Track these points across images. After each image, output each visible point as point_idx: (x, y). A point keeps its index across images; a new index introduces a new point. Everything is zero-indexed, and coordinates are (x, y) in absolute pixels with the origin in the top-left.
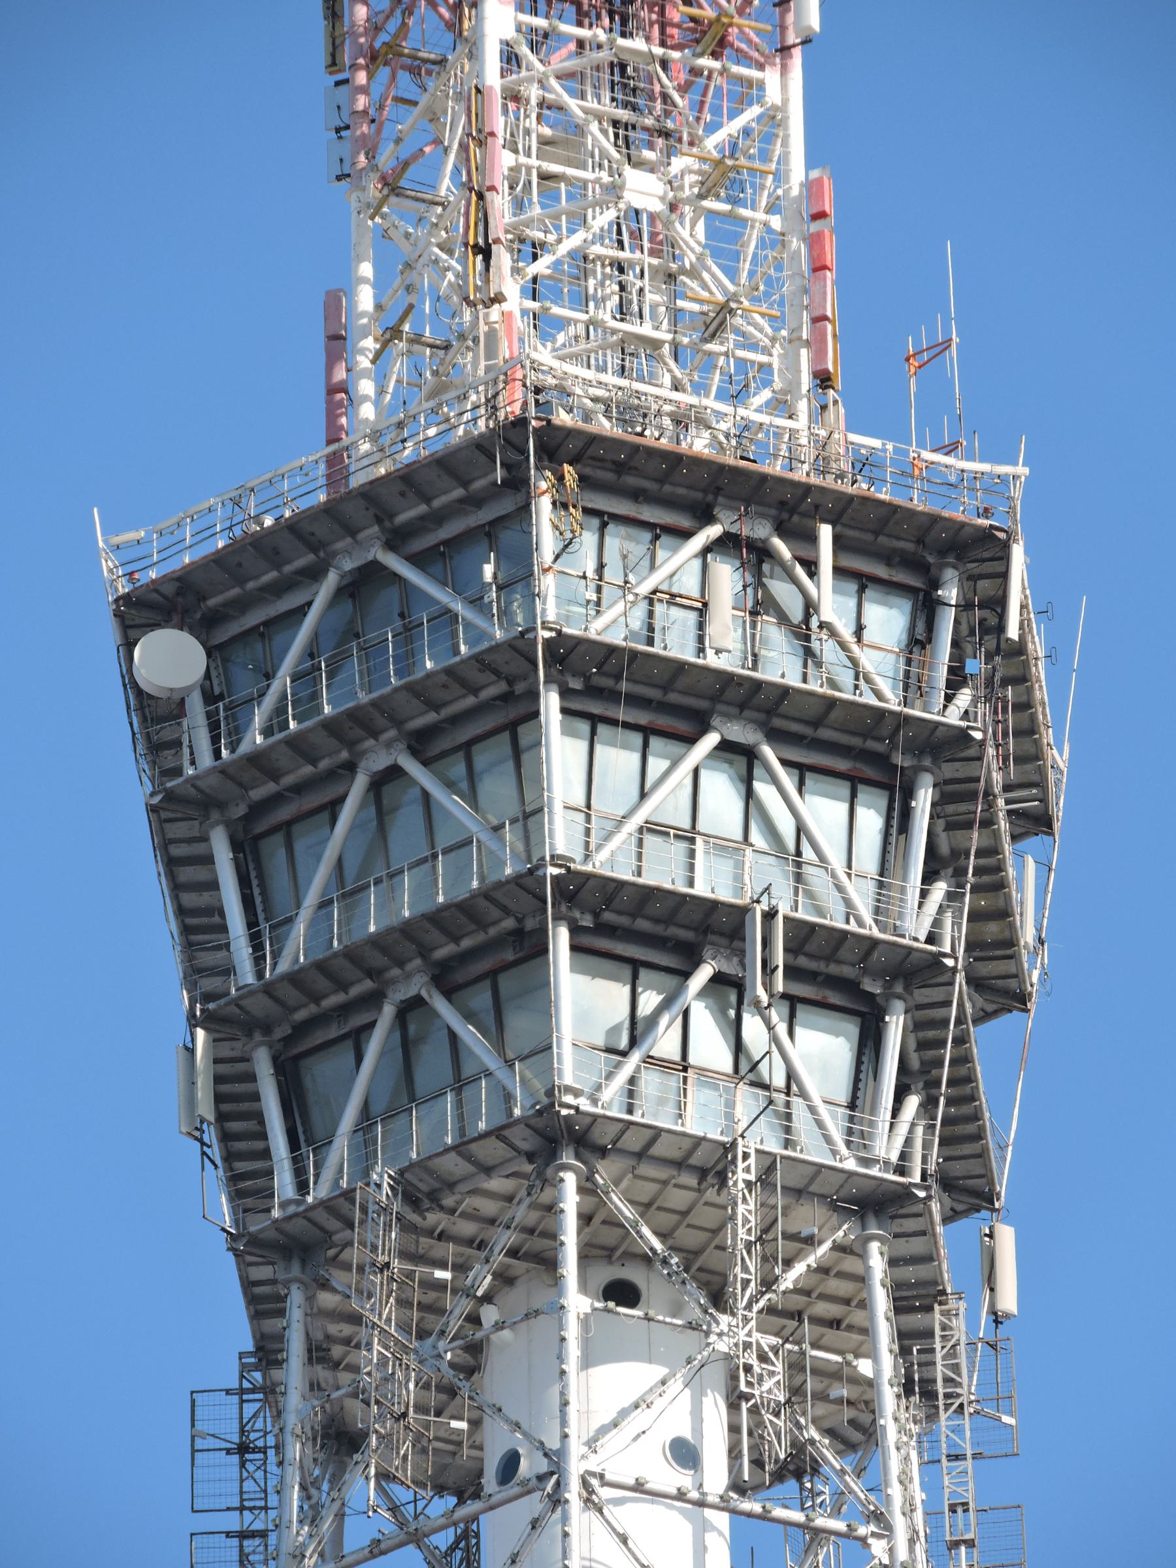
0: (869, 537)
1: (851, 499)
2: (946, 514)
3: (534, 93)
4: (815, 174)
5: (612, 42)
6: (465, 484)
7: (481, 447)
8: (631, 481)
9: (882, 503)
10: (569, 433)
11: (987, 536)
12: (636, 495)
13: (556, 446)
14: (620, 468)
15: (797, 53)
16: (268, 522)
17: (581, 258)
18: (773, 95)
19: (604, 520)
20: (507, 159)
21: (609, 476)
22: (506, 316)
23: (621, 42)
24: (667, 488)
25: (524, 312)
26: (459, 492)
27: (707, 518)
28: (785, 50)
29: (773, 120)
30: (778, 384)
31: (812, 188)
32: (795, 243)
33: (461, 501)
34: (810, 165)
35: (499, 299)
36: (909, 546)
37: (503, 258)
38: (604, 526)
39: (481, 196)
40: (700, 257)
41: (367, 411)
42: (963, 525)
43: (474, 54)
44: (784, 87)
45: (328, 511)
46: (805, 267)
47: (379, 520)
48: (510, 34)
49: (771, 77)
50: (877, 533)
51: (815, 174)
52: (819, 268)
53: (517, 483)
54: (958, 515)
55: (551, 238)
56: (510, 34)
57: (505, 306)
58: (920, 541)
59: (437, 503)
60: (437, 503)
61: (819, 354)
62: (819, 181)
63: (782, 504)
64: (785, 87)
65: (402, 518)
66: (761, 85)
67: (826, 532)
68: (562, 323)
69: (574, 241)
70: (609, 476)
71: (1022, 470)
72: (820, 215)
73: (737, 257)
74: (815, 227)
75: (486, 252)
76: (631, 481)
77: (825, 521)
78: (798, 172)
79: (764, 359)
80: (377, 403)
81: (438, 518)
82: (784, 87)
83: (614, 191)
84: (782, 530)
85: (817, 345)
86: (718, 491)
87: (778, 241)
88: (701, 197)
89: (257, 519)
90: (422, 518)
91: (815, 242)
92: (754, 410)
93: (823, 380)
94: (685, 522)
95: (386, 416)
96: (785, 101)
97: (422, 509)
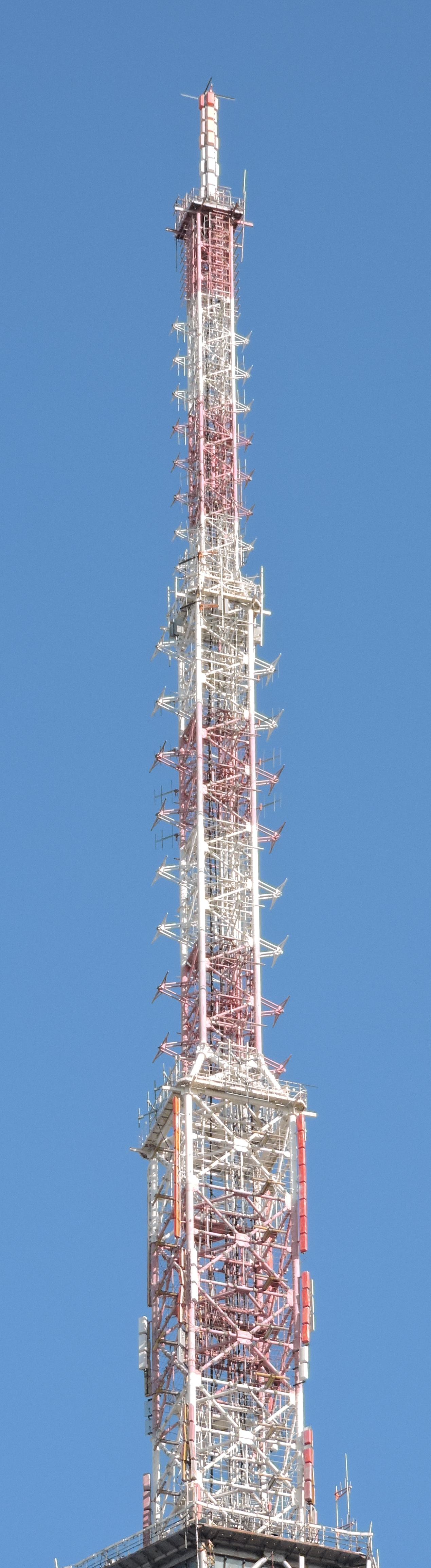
0: (317, 1559)
1: (310, 1547)
2: (344, 1551)
3: (210, 1404)
4: (306, 1429)
5: (235, 1386)
6: (177, 1547)
7: (181, 1535)
8: (234, 1544)
9: (321, 1548)
10: (211, 1529)
11: (359, 1558)
12: (237, 1549)
13: (206, 1534)
14: (230, 1540)
15: (301, 1386)
16: (113, 1561)
17: (228, 1461)
18: (292, 1402)
19: (225, 1558)
20: (198, 1428)
21: (226, 1543)
22: (197, 1485)
23: (238, 1385)
24: (247, 1546)
25: (205, 1483)
26: (175, 1550)
27: (261, 1555)
28: (296, 1385)
29: (293, 1409)
30: (293, 1503)
31: (305, 1434)
32: (300, 1453)
33: (177, 1553)
34: (305, 1426)
35: (193, 1479)
36: (333, 1562)
37: (194, 1463)
38: (225, 1560)
39: (188, 1443)
40: (266, 1460)
41: (158, 1516)
42: (350, 1554)
43: (186, 1394)
44: (296, 1398)
45: (143, 1552)
46: (303, 1461)
47: (149, 1561)
48: (199, 1384)
49: (291, 1395)
50: (321, 1558)
51: (306, 1429)
52: (308, 1462)
53: (193, 1547)
54: (349, 1551)
55: (216, 1454)
56: (199, 1384)
57: (196, 1482)
58: (337, 1560)
59: (168, 1554)
60: (168, 1554)
61: (307, 1493)
62: (307, 1432)
63: (287, 1550)
64: (297, 1398)
65: (157, 1559)
66: (288, 1398)
67: (302, 1559)
68: (219, 1487)
69: (224, 1455)
70: (226, 1543)
71: (371, 1534)
72: (308, 1443)
73: (282, 1460)
74: (306, 1447)
75: (189, 1463)
76: (234, 1544)
77: (302, 1555)
78: (301, 1428)
79: (288, 1495)
80: (161, 1513)
81: (170, 1559)
82: (296, 1398)
83: (237, 1438)
84: (288, 1559)
85: (307, 1489)
86: (265, 1546)
87: (293, 1453)
88: (267, 1439)
89: (109, 1561)
90: (164, 1559)
91: (306, 1453)
92: (277, 1518)
93: (309, 1502)
94: (254, 1557)
95: (163, 1519)
96: (297, 1403)
97: (164, 1556)
